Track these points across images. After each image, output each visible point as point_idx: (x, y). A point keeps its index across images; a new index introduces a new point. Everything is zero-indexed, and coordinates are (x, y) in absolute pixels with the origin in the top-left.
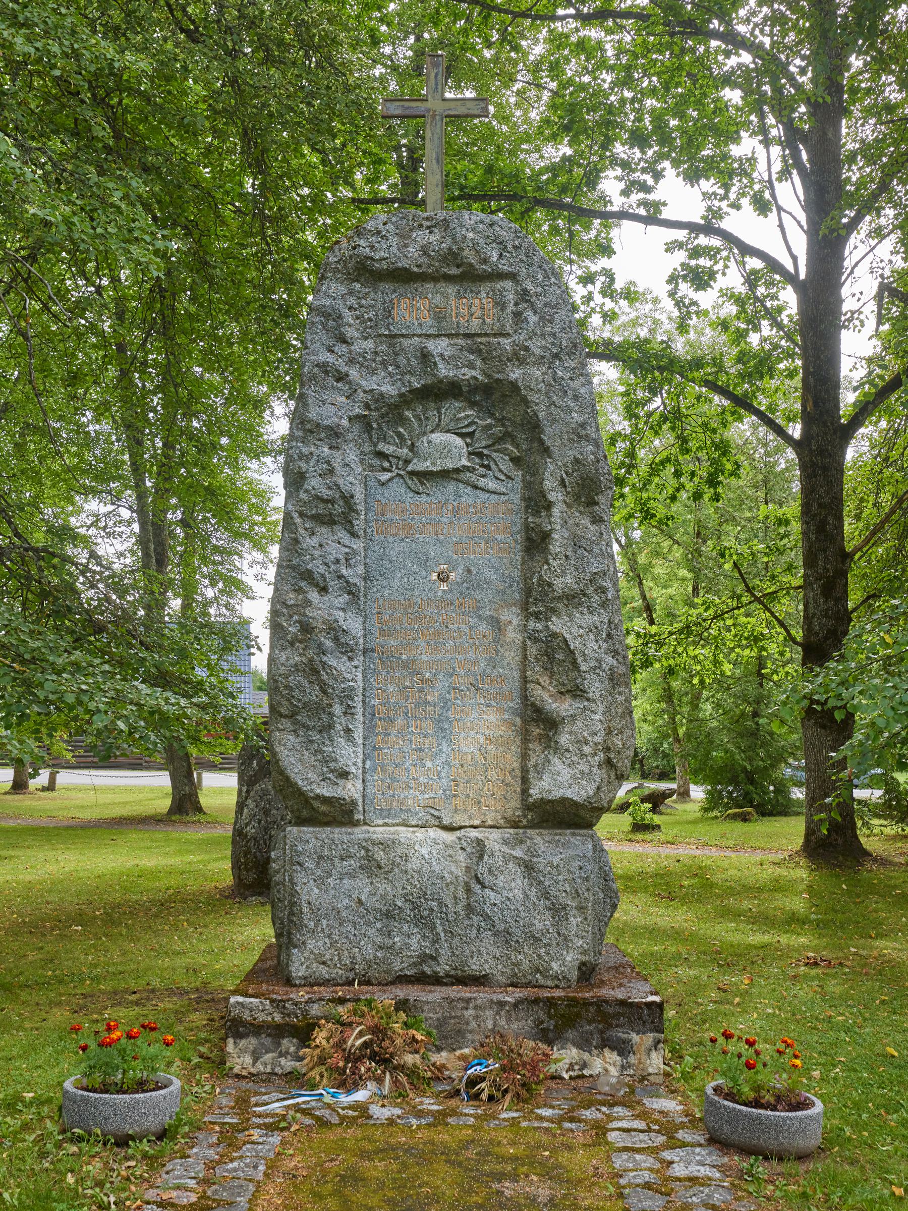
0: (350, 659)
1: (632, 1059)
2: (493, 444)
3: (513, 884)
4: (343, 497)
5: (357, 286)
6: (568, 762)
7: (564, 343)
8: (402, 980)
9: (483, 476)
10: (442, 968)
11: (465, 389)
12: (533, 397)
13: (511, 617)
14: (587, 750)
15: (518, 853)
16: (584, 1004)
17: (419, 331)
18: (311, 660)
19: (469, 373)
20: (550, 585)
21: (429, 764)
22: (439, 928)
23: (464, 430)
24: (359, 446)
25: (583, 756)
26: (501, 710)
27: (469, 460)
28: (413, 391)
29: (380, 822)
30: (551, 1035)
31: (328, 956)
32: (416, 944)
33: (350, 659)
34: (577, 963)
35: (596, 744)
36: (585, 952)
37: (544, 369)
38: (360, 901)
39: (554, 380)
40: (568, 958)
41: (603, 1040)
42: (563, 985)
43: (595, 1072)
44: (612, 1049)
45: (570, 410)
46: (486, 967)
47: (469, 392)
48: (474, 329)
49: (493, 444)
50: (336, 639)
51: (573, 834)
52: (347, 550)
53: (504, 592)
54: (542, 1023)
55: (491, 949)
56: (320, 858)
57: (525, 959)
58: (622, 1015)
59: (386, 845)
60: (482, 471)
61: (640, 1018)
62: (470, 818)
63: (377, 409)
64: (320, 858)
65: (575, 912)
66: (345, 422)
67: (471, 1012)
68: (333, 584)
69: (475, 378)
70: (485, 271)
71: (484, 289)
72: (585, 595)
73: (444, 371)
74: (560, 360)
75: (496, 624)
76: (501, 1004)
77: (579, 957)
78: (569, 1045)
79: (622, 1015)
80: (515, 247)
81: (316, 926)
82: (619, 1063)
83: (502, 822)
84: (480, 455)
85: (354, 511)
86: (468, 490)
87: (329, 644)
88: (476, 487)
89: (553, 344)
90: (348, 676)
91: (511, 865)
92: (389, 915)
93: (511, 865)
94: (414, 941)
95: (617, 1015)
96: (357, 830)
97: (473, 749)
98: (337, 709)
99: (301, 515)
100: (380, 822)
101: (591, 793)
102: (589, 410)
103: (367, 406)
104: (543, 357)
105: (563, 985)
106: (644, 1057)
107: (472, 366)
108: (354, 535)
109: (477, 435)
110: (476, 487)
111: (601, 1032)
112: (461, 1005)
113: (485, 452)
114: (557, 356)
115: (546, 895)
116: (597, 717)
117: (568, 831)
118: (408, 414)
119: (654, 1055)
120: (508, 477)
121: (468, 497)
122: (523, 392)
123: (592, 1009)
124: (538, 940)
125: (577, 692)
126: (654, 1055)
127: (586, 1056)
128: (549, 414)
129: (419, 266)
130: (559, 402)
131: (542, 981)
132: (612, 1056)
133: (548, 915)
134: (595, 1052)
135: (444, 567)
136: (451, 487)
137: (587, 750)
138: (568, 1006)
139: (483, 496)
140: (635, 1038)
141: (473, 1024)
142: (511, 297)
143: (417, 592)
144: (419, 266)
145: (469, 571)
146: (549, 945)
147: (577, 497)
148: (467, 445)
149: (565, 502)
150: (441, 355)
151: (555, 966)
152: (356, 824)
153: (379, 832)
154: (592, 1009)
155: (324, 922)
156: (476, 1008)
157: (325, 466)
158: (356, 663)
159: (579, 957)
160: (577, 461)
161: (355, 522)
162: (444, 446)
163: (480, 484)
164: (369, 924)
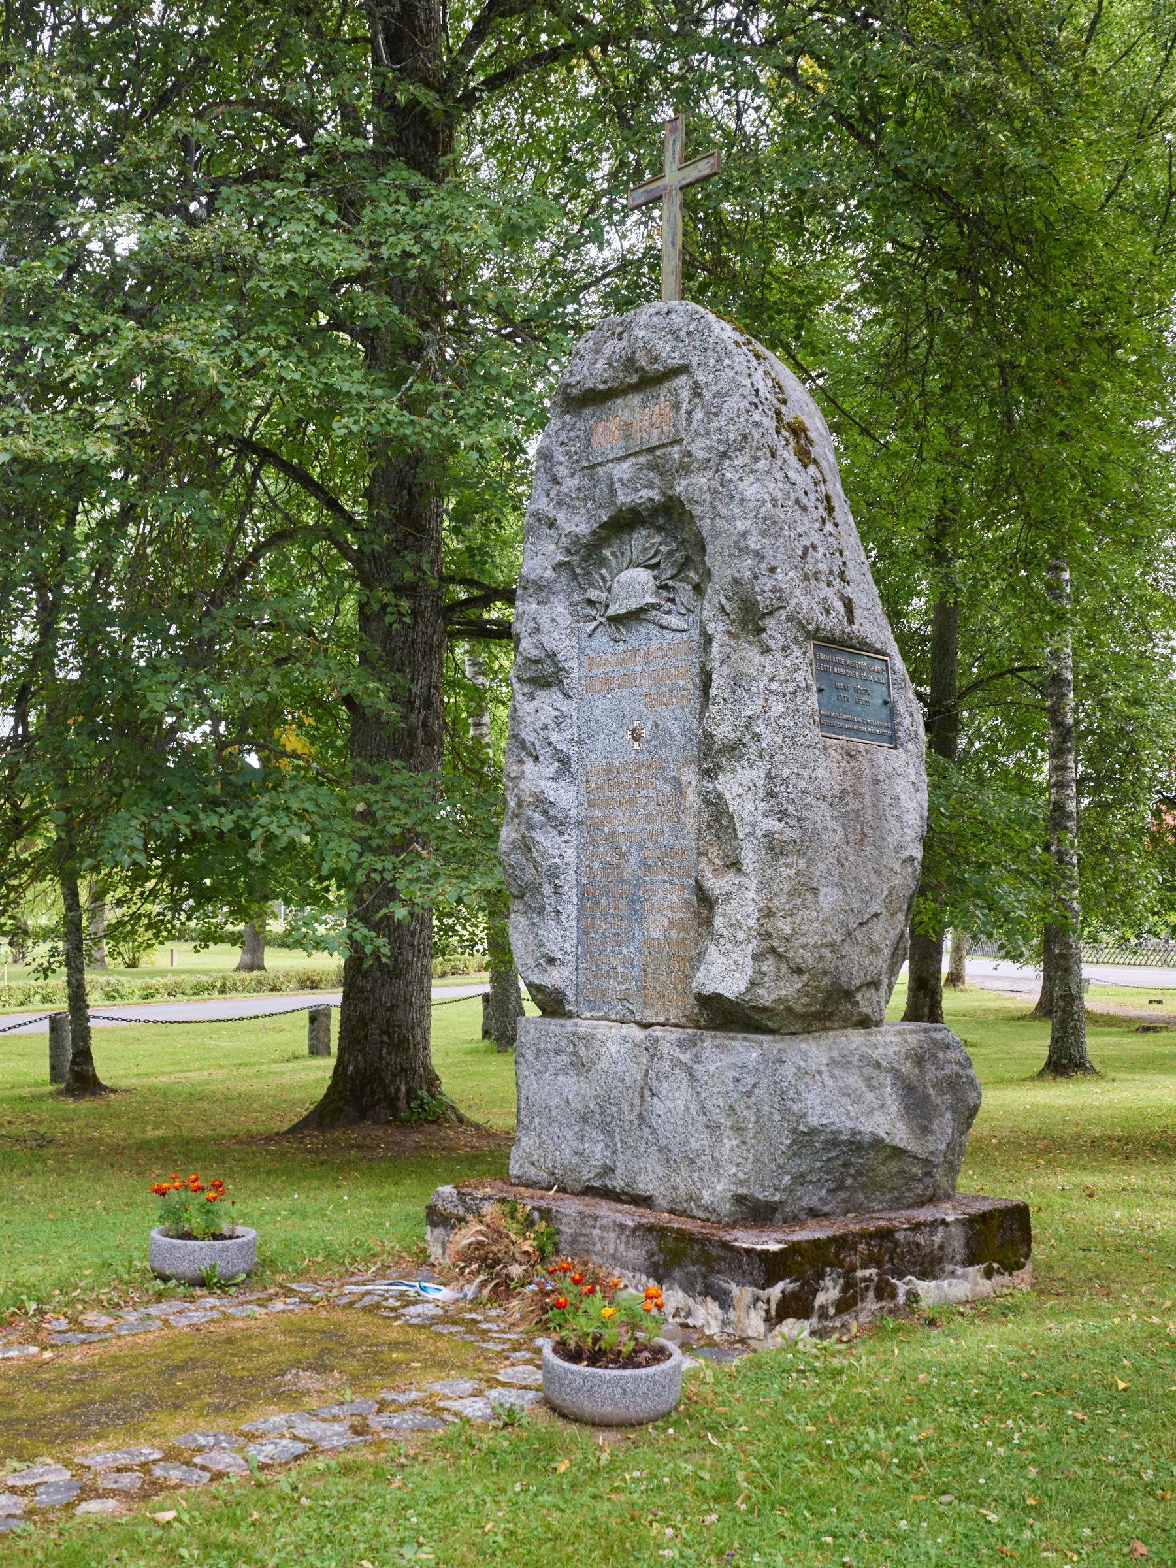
0: (561, 833)
1: (732, 1315)
2: (679, 572)
3: (677, 1094)
4: (548, 656)
5: (568, 417)
6: (723, 949)
7: (732, 437)
8: (588, 1191)
9: (668, 613)
10: (617, 1183)
11: (645, 514)
12: (697, 511)
13: (690, 776)
14: (741, 935)
15: (685, 1058)
16: (691, 1240)
17: (611, 456)
18: (524, 836)
19: (646, 493)
20: (712, 735)
21: (625, 951)
22: (618, 1138)
23: (653, 562)
24: (569, 596)
25: (738, 943)
26: (682, 888)
27: (657, 595)
28: (603, 526)
29: (588, 1014)
30: (661, 1271)
31: (536, 1157)
32: (598, 1154)
33: (561, 833)
34: (729, 1195)
35: (750, 928)
36: (741, 1183)
37: (710, 474)
38: (568, 1101)
39: (722, 485)
40: (719, 1188)
41: (706, 1286)
42: (713, 1219)
43: (699, 1323)
44: (715, 1298)
45: (734, 518)
46: (651, 1187)
47: (650, 515)
48: (654, 442)
49: (679, 572)
50: (545, 812)
51: (745, 1039)
52: (557, 713)
53: (684, 748)
54: (653, 1255)
55: (657, 1167)
56: (538, 1050)
57: (682, 1181)
58: (724, 1259)
59: (588, 1039)
60: (667, 606)
61: (740, 1267)
62: (657, 1014)
63: (577, 552)
64: (538, 1050)
65: (728, 1132)
66: (549, 573)
67: (596, 1232)
68: (545, 752)
69: (651, 500)
70: (657, 370)
71: (663, 392)
72: (744, 745)
73: (624, 498)
74: (730, 458)
75: (677, 784)
76: (622, 1227)
77: (733, 1187)
78: (676, 1286)
79: (724, 1259)
80: (688, 333)
81: (531, 1122)
82: (720, 1317)
83: (684, 1020)
84: (666, 587)
85: (563, 669)
86: (657, 631)
87: (538, 818)
88: (662, 627)
89: (720, 441)
90: (555, 852)
91: (677, 1071)
92: (584, 1119)
93: (677, 1071)
94: (598, 1150)
95: (719, 1259)
96: (568, 1022)
97: (658, 934)
98: (547, 889)
99: (520, 680)
100: (588, 1014)
101: (743, 989)
102: (752, 515)
103: (568, 551)
104: (709, 460)
105: (713, 1219)
106: (743, 1315)
107: (650, 486)
108: (567, 696)
109: (662, 565)
110: (662, 627)
111: (705, 1277)
112: (590, 1222)
113: (670, 583)
114: (724, 455)
115: (704, 1111)
116: (751, 895)
117: (740, 1036)
118: (606, 552)
119: (753, 1313)
120: (688, 610)
121: (658, 640)
122: (688, 507)
123: (697, 1247)
124: (692, 1162)
125: (735, 865)
126: (753, 1313)
127: (690, 1302)
128: (714, 527)
129: (605, 382)
130: (725, 512)
131: (695, 1212)
132: (713, 1307)
133: (706, 1134)
134: (699, 1299)
135: (636, 723)
136: (643, 629)
137: (741, 935)
138: (676, 1239)
139: (668, 635)
140: (735, 1289)
141: (598, 1247)
142: (685, 394)
143: (615, 755)
144: (605, 382)
145: (656, 726)
146: (702, 1169)
147: (744, 624)
148: (655, 578)
149: (729, 632)
150: (621, 480)
151: (706, 1194)
152: (570, 1015)
153: (583, 1026)
154: (697, 1247)
155: (537, 1120)
156: (602, 1228)
157: (532, 624)
158: (566, 837)
159: (733, 1187)
160: (735, 581)
161: (566, 681)
162: (634, 584)
163: (665, 623)
164: (570, 1126)
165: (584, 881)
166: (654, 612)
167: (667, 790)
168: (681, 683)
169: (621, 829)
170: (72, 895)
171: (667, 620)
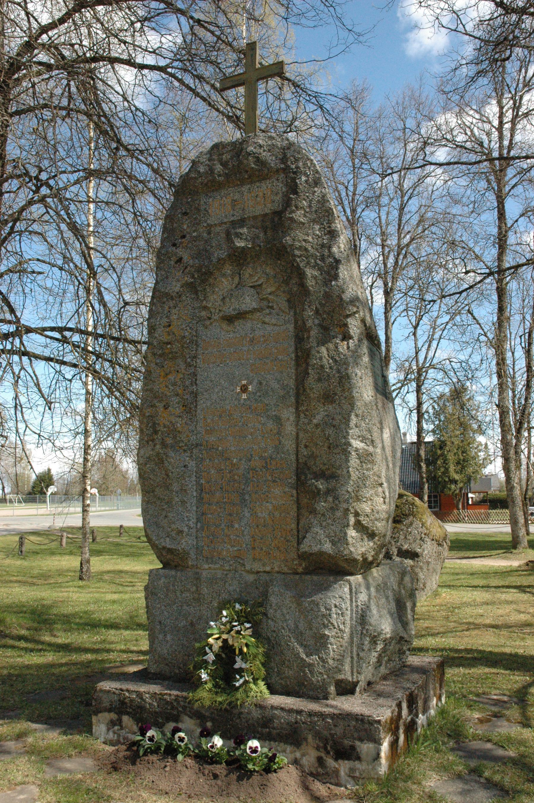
13: (288, 414)
75: (278, 420)
100: (206, 566)
143: (227, 402)
145: (261, 383)
166: (258, 314)
167: (270, 425)
168: (280, 357)
169: (233, 449)
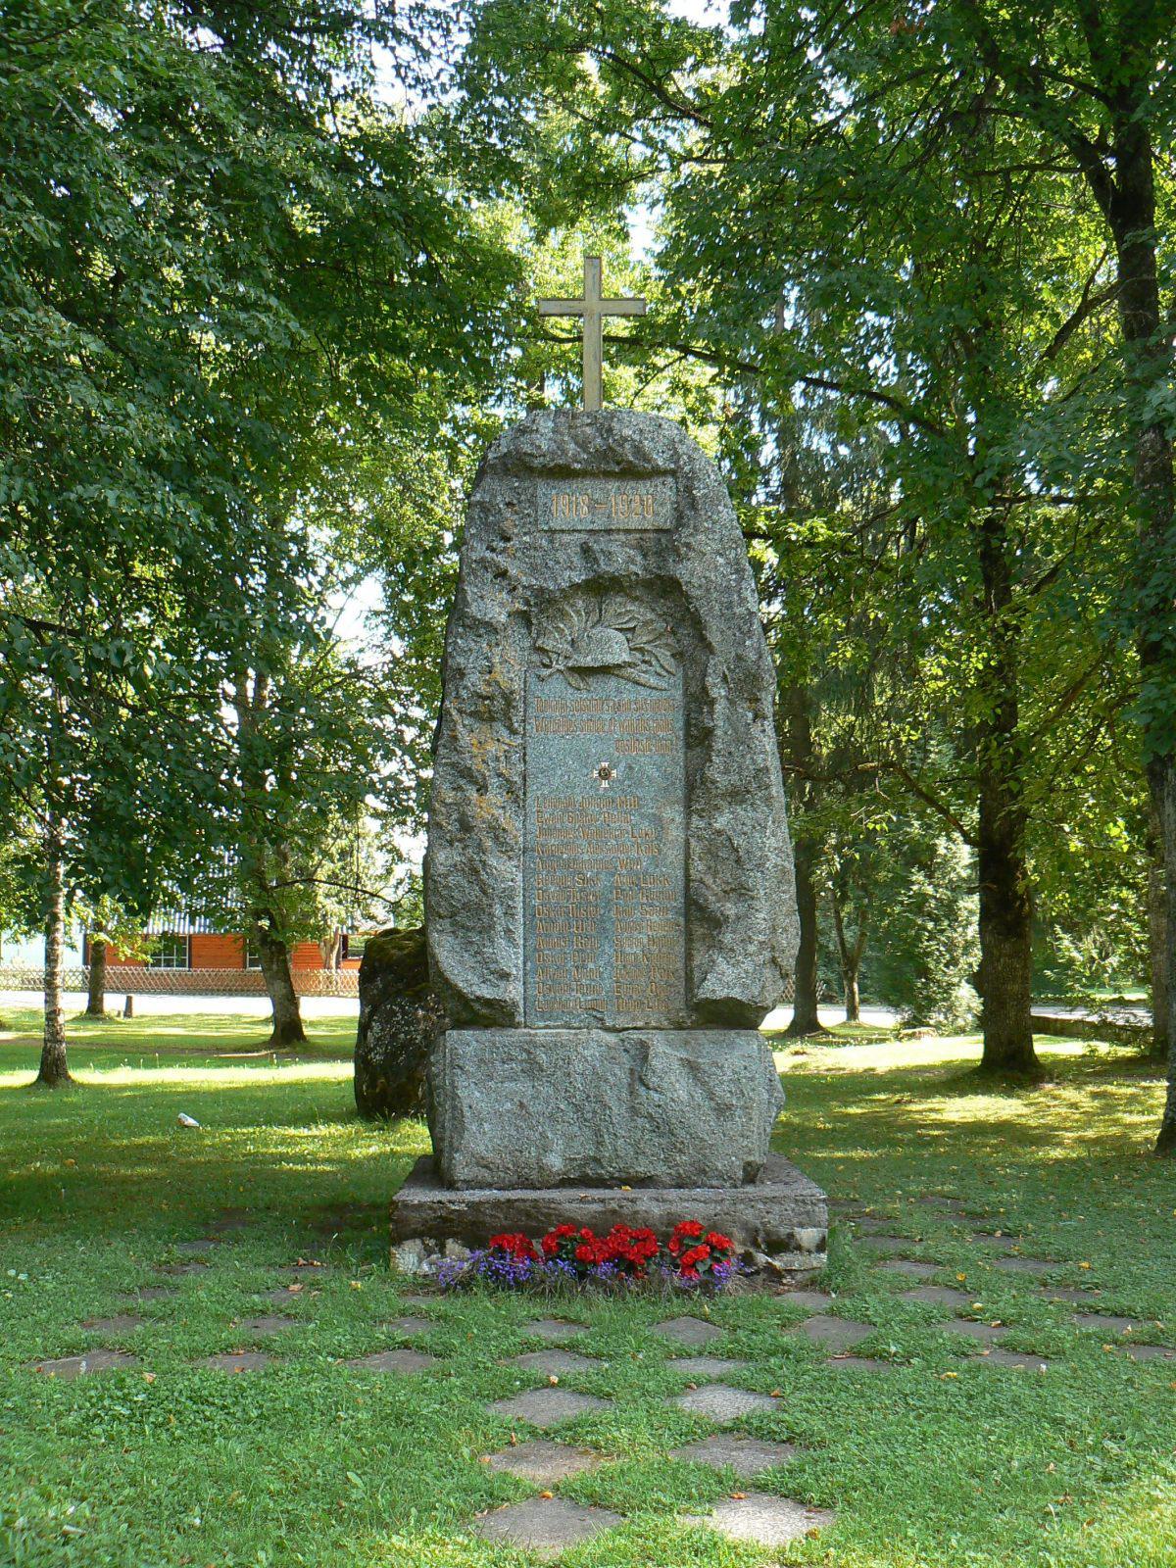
13: (674, 814)
18: (471, 860)
29: (542, 1024)
72: (748, 792)
75: (657, 820)
85: (676, 550)
98: (498, 910)
100: (542, 1024)
110: (638, 683)
113: (647, 647)
121: (629, 693)
136: (613, 683)
143: (577, 790)
145: (631, 768)
152: (517, 1026)
163: (642, 681)
165: (536, 902)
166: (630, 670)
167: (645, 826)
170: (997, 111)
171: (644, 678)
